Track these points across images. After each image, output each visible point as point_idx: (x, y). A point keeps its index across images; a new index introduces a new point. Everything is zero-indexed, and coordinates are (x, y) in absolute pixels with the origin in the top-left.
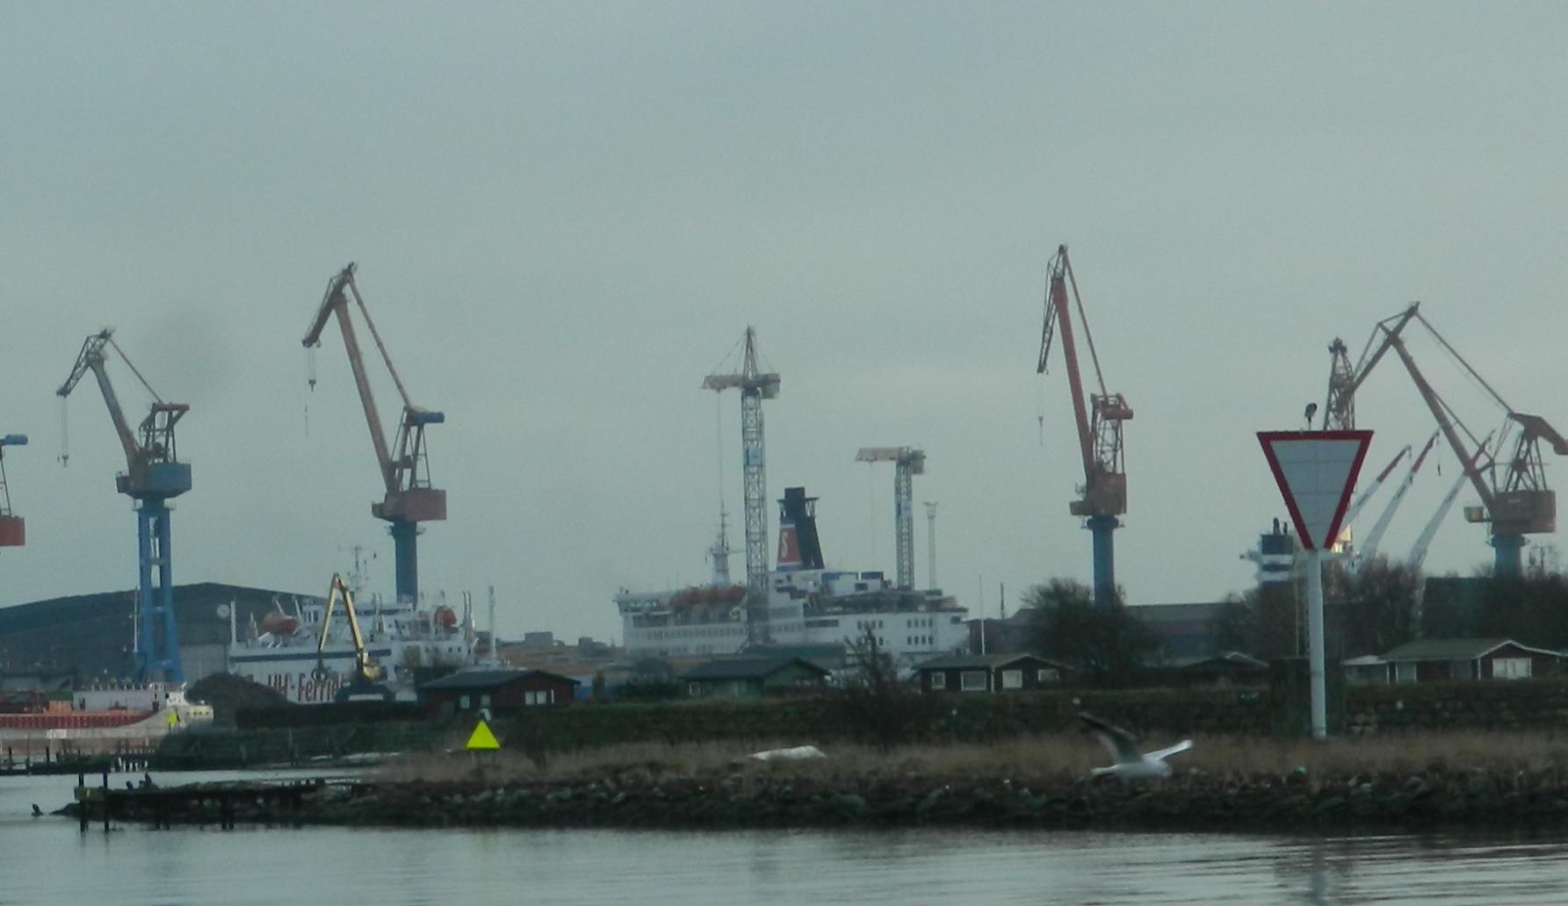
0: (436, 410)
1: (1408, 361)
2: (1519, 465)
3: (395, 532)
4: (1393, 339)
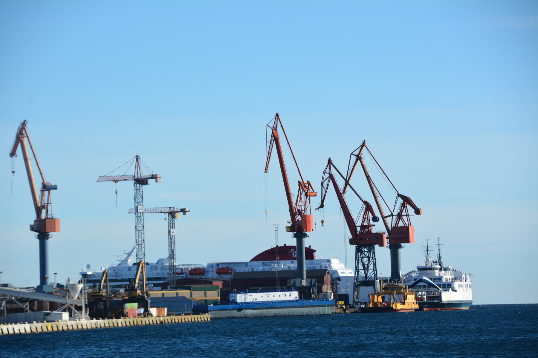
0: (53, 184)
1: (363, 166)
2: (400, 216)
3: (39, 237)
4: (359, 158)
